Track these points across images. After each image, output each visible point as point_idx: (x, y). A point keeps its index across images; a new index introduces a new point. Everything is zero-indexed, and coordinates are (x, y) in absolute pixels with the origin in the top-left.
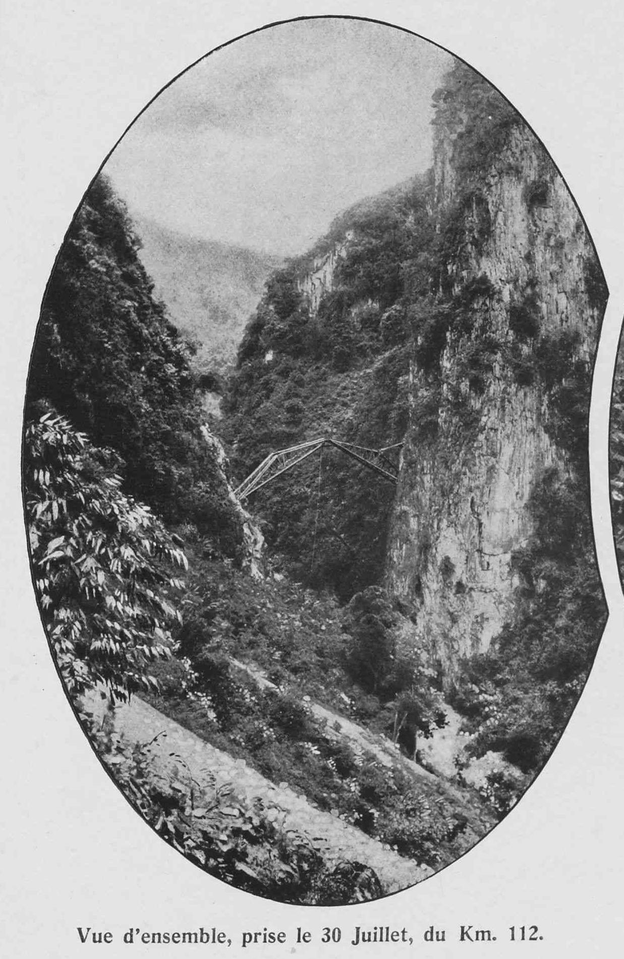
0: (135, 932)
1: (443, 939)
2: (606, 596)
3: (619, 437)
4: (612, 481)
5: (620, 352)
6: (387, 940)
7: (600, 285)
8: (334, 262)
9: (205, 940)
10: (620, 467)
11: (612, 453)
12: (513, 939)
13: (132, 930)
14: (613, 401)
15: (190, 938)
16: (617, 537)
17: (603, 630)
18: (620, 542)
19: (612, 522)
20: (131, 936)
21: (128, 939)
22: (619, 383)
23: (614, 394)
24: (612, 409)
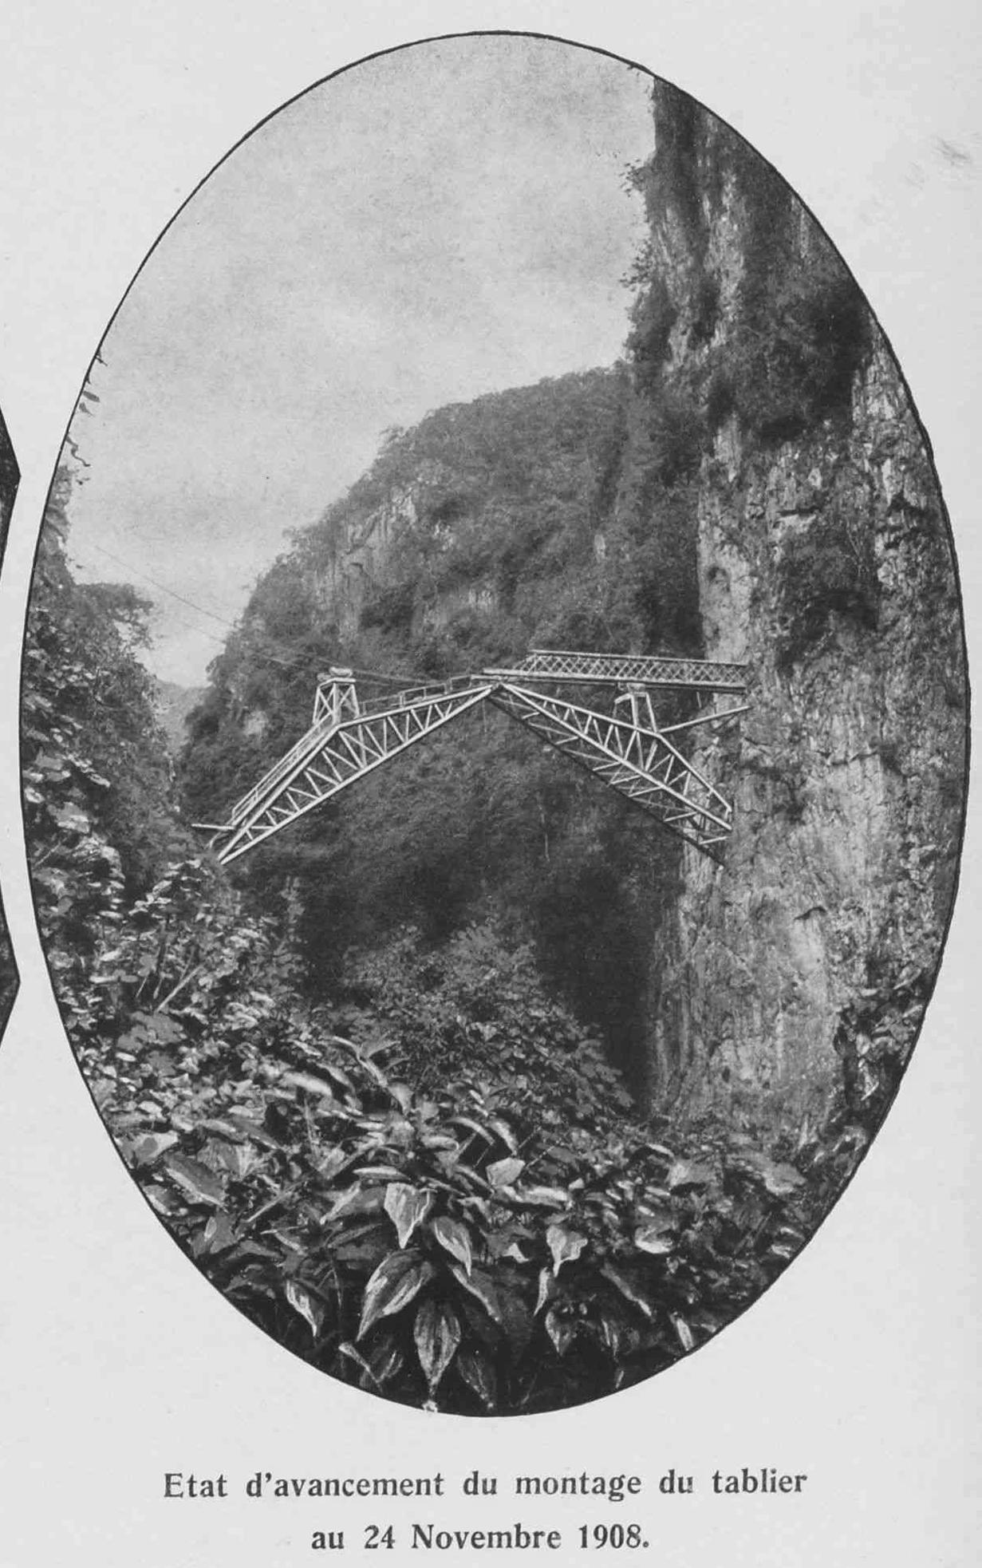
0: (264, 1479)
1: (493, 1492)
2: (16, 953)
3: (36, 703)
4: (25, 772)
5: (38, 568)
6: (773, 1490)
7: (7, 461)
8: (390, 531)
9: (750, 1486)
10: (38, 750)
11: (25, 728)
12: (584, 1545)
13: (259, 1475)
14: (26, 646)
15: (500, 1540)
16: (32, 860)
17: (11, 1008)
18: (38, 869)
19: (26, 837)
20: (259, 1485)
21: (254, 1490)
22: (36, 617)
23: (28, 635)
24: (25, 658)
